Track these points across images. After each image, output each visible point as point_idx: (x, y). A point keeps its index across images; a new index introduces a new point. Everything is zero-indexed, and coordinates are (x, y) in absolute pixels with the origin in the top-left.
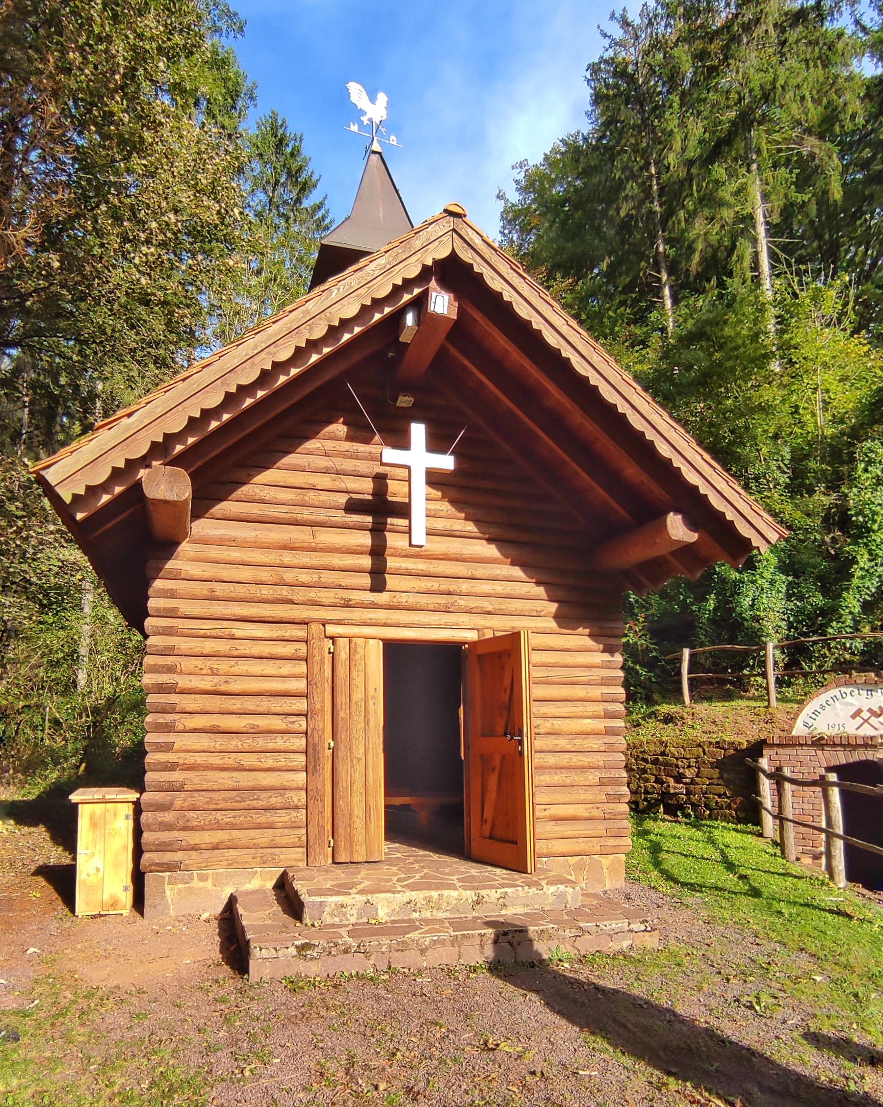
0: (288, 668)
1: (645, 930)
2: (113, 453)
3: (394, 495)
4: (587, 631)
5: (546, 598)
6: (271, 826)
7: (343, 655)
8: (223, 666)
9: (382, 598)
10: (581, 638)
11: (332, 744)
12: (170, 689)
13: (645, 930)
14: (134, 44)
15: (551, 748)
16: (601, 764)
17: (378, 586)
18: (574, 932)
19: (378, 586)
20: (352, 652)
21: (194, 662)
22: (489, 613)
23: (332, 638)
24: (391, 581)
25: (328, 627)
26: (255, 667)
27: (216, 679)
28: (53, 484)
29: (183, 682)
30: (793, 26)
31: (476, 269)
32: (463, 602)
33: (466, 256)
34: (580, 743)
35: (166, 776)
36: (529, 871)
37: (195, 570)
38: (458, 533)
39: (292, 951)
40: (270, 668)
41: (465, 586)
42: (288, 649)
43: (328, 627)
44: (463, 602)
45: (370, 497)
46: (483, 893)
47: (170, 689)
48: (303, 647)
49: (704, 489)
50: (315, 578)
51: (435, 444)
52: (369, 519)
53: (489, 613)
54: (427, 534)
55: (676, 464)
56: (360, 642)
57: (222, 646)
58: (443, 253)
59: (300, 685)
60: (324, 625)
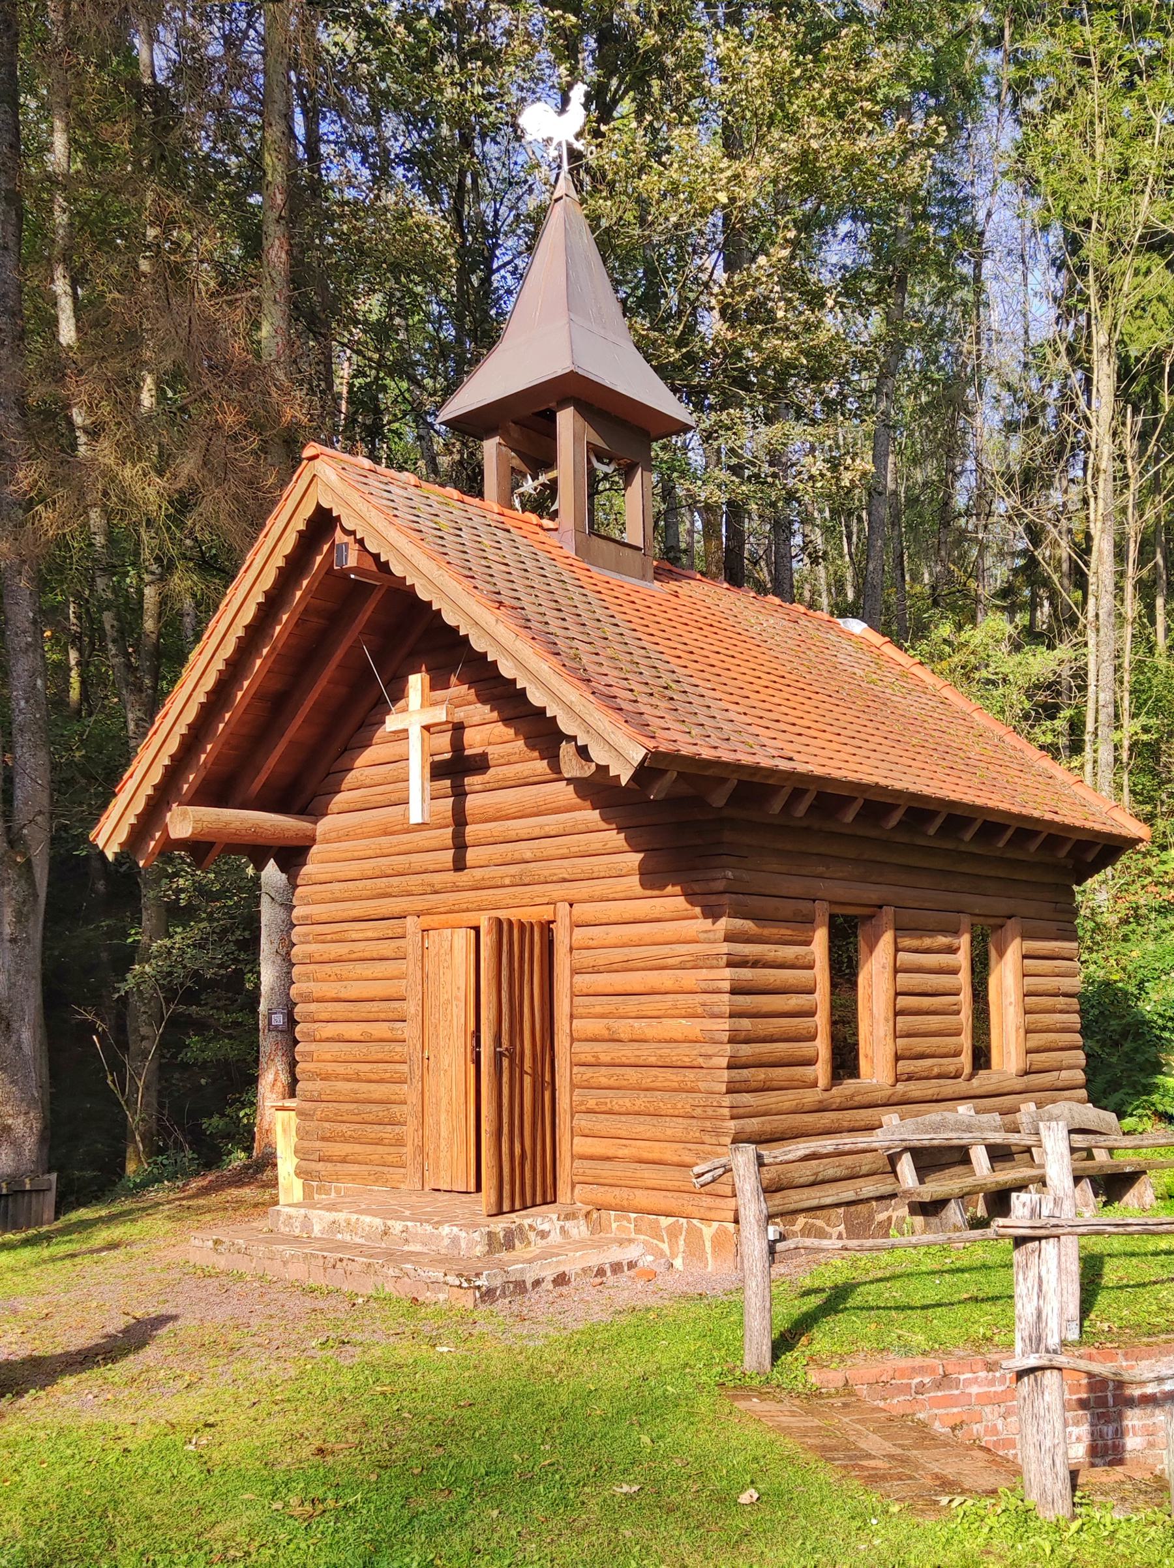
1: (460, 1286)
3: (471, 747)
4: (678, 889)
5: (627, 848)
6: (379, 1142)
9: (463, 877)
10: (673, 901)
13: (460, 1286)
14: (560, 58)
15: (633, 1061)
17: (459, 865)
18: (397, 1273)
19: (459, 865)
21: (327, 968)
22: (565, 880)
24: (471, 855)
30: (462, 135)
35: (319, 1085)
38: (531, 780)
39: (210, 1244)
45: (448, 756)
46: (390, 1223)
52: (448, 783)
53: (565, 880)
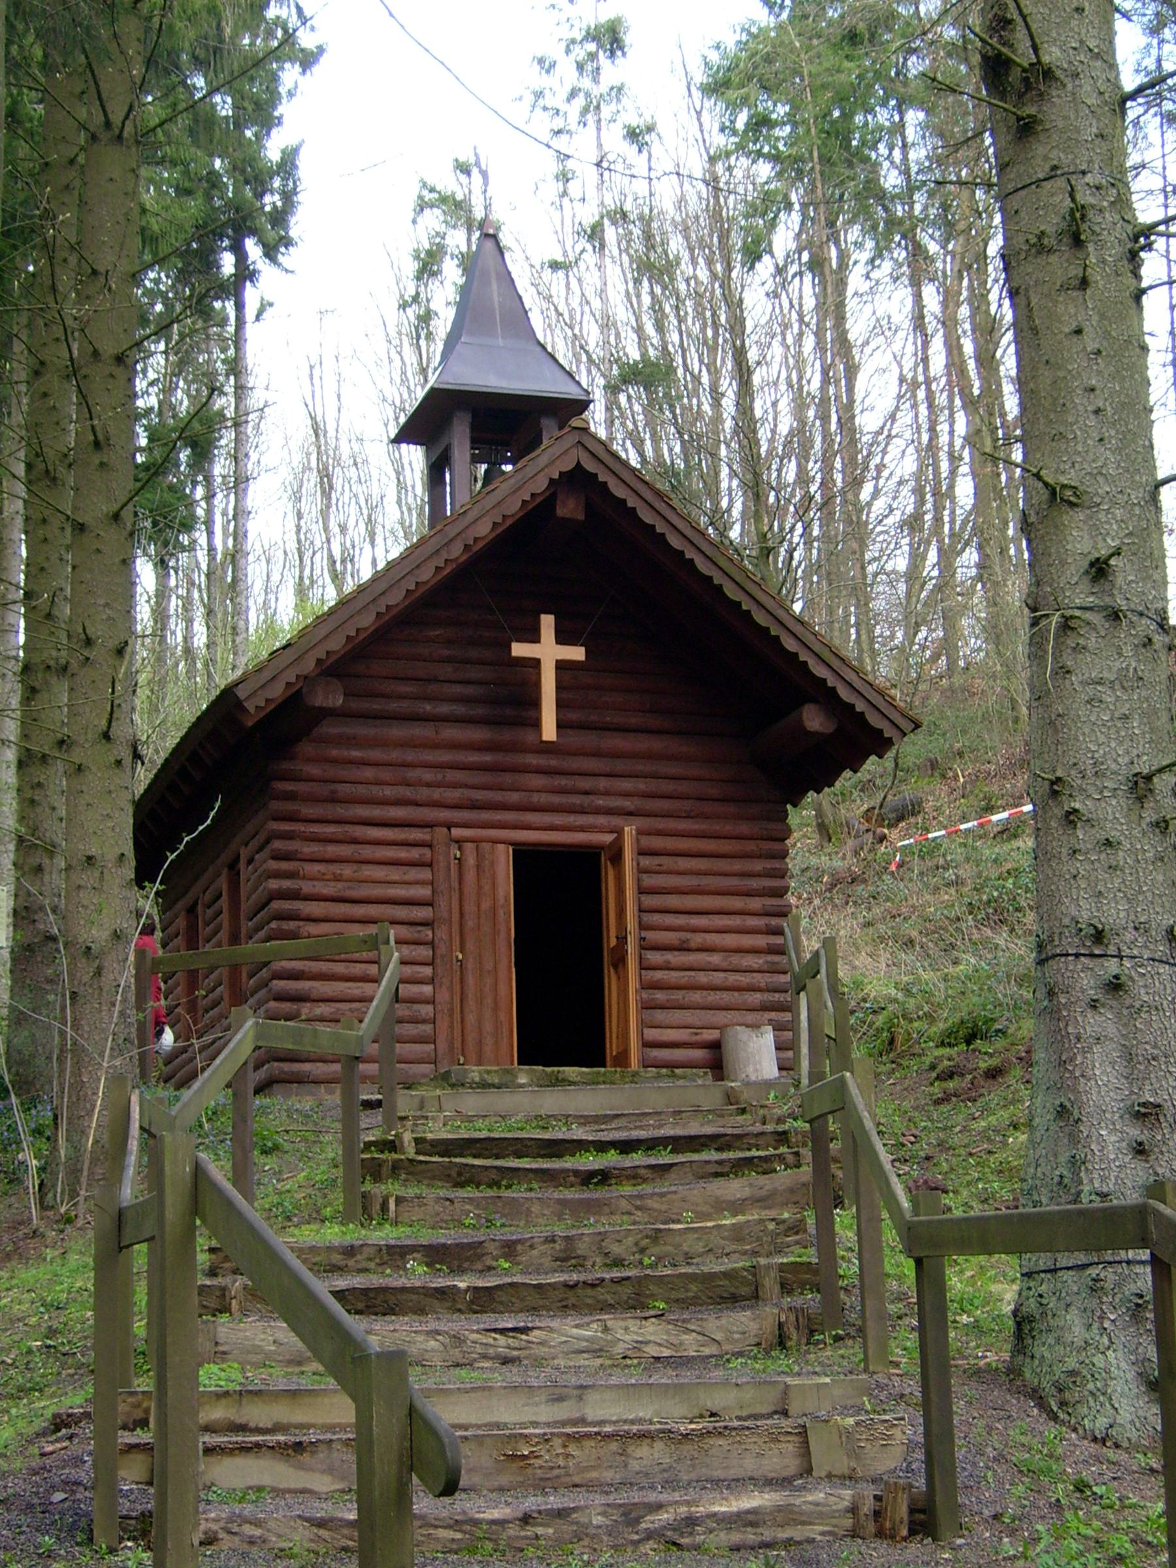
0: (413, 874)
2: (288, 671)
7: (471, 860)
8: (347, 871)
11: (460, 957)
12: (295, 895)
16: (763, 985)
20: (480, 856)
23: (457, 842)
25: (453, 830)
26: (379, 873)
27: (340, 885)
28: (242, 698)
29: (307, 887)
31: (601, 478)
32: (601, 802)
33: (590, 466)
34: (736, 960)
36: (608, 838)
37: (315, 770)
40: (395, 874)
41: (603, 783)
42: (414, 854)
43: (453, 830)
44: (601, 802)
47: (295, 895)
48: (427, 851)
49: (831, 681)
50: (440, 777)
51: (563, 638)
54: (777, 1049)
55: (803, 657)
56: (486, 846)
57: (345, 850)
58: (568, 465)
59: (424, 892)
60: (449, 829)
